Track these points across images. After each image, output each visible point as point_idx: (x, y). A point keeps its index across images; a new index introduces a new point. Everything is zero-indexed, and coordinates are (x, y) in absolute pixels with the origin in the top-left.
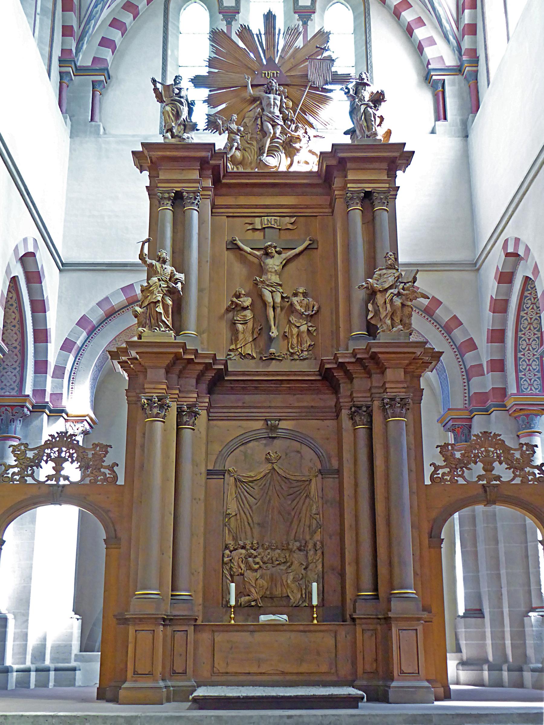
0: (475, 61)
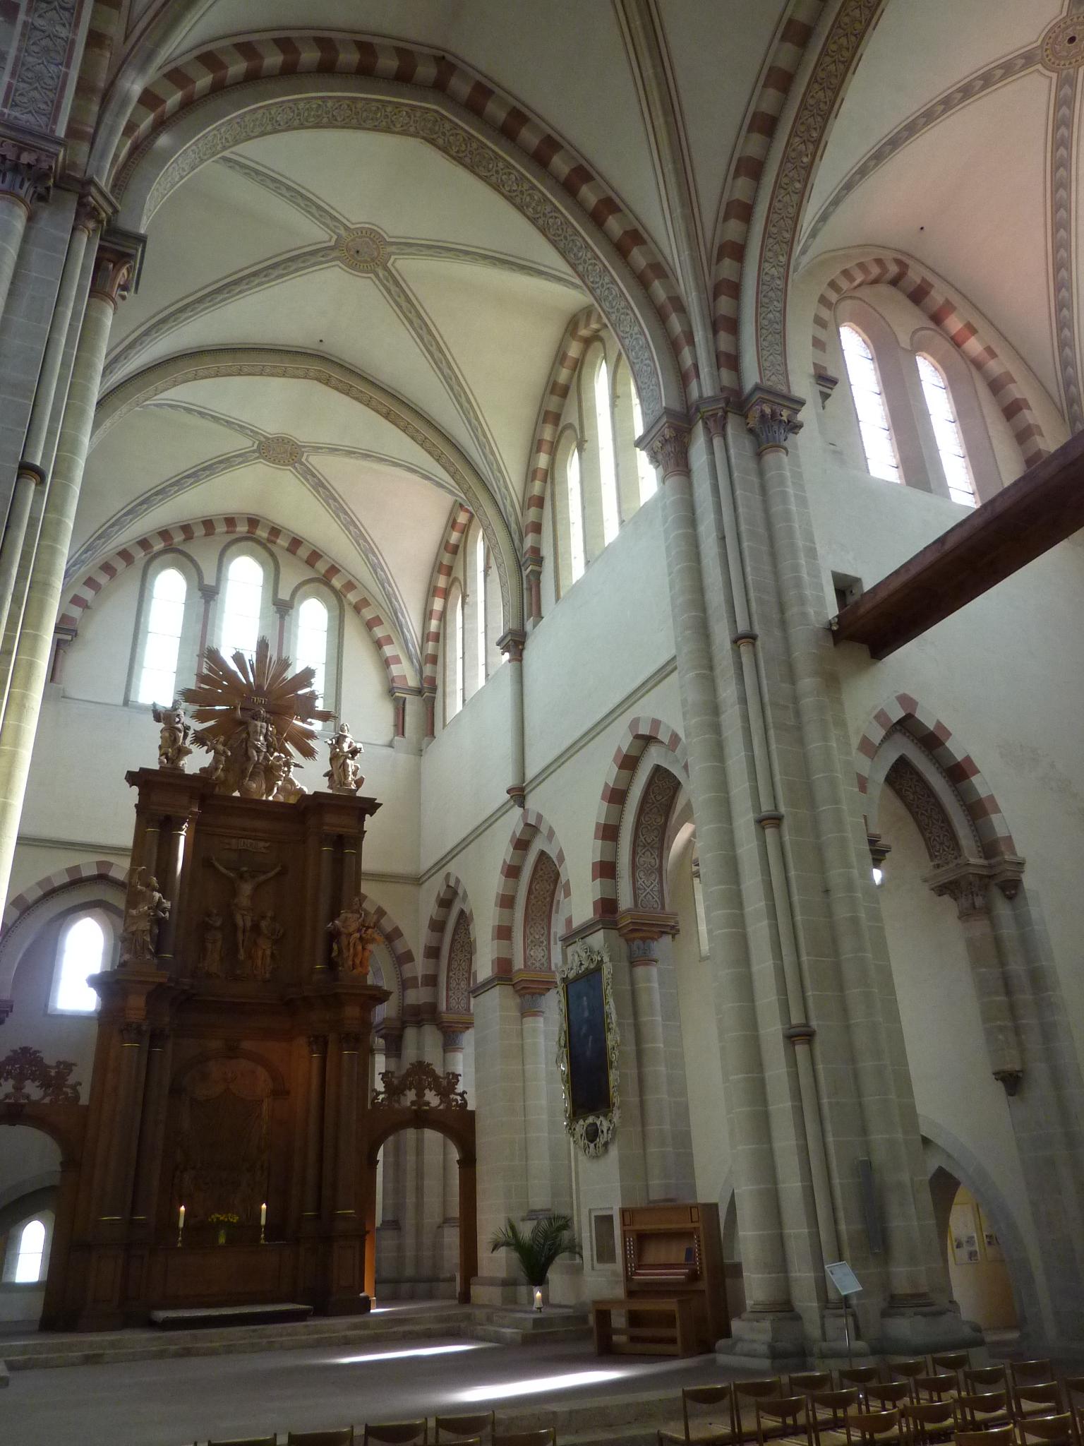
0: (434, 689)
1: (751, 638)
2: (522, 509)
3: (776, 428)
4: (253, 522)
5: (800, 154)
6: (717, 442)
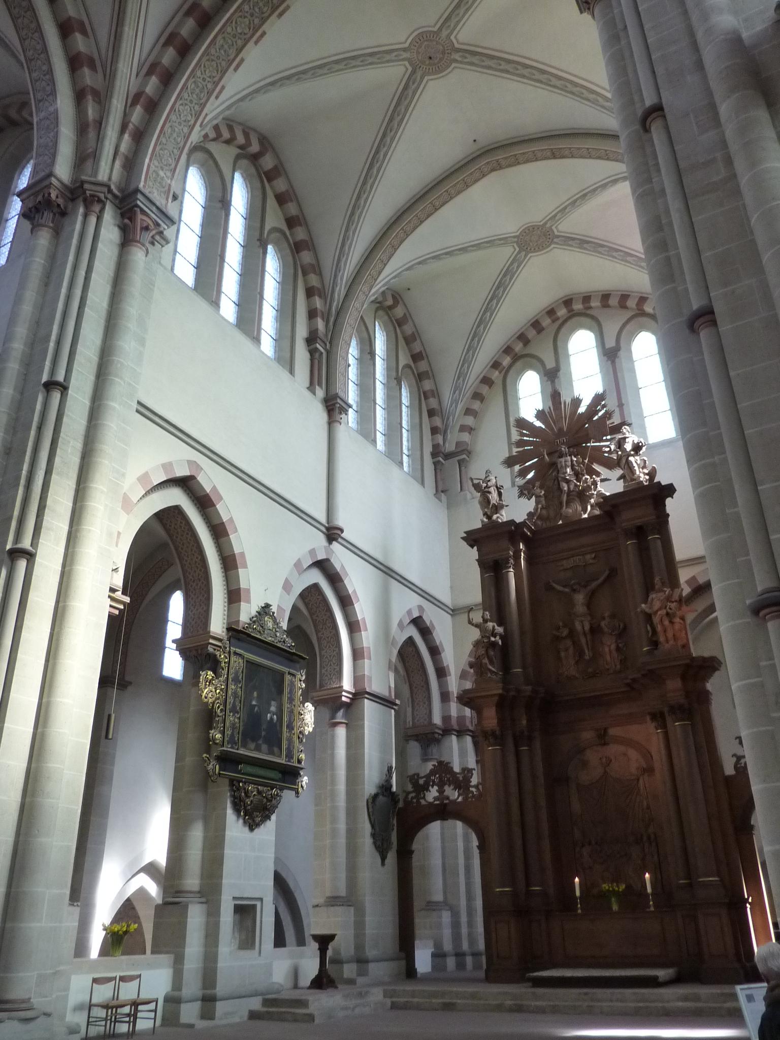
1: (658, 109)
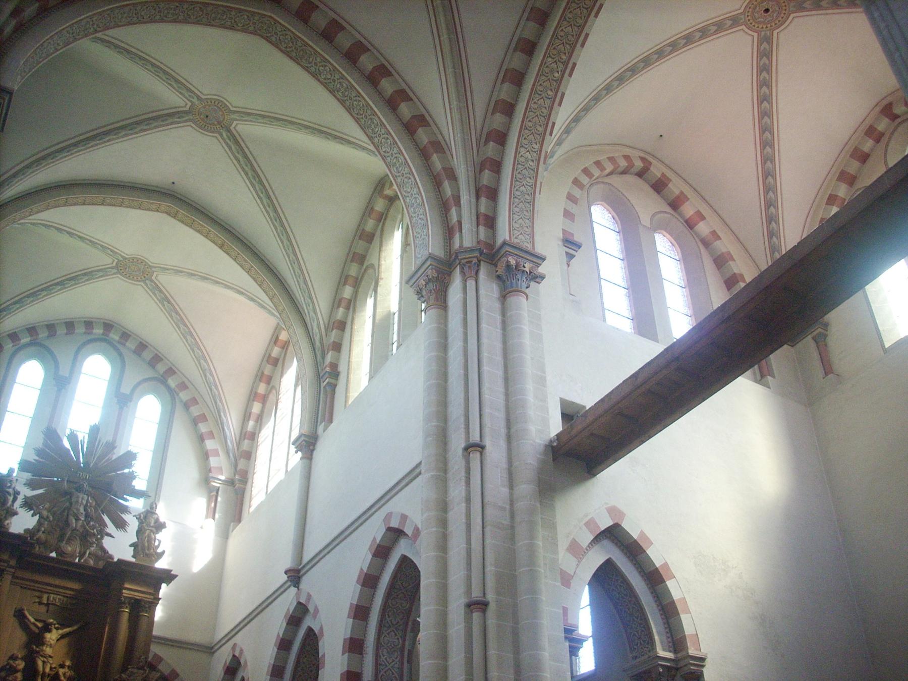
2: (326, 330)
3: (519, 276)
4: (108, 326)
5: (552, 71)
6: (471, 283)
